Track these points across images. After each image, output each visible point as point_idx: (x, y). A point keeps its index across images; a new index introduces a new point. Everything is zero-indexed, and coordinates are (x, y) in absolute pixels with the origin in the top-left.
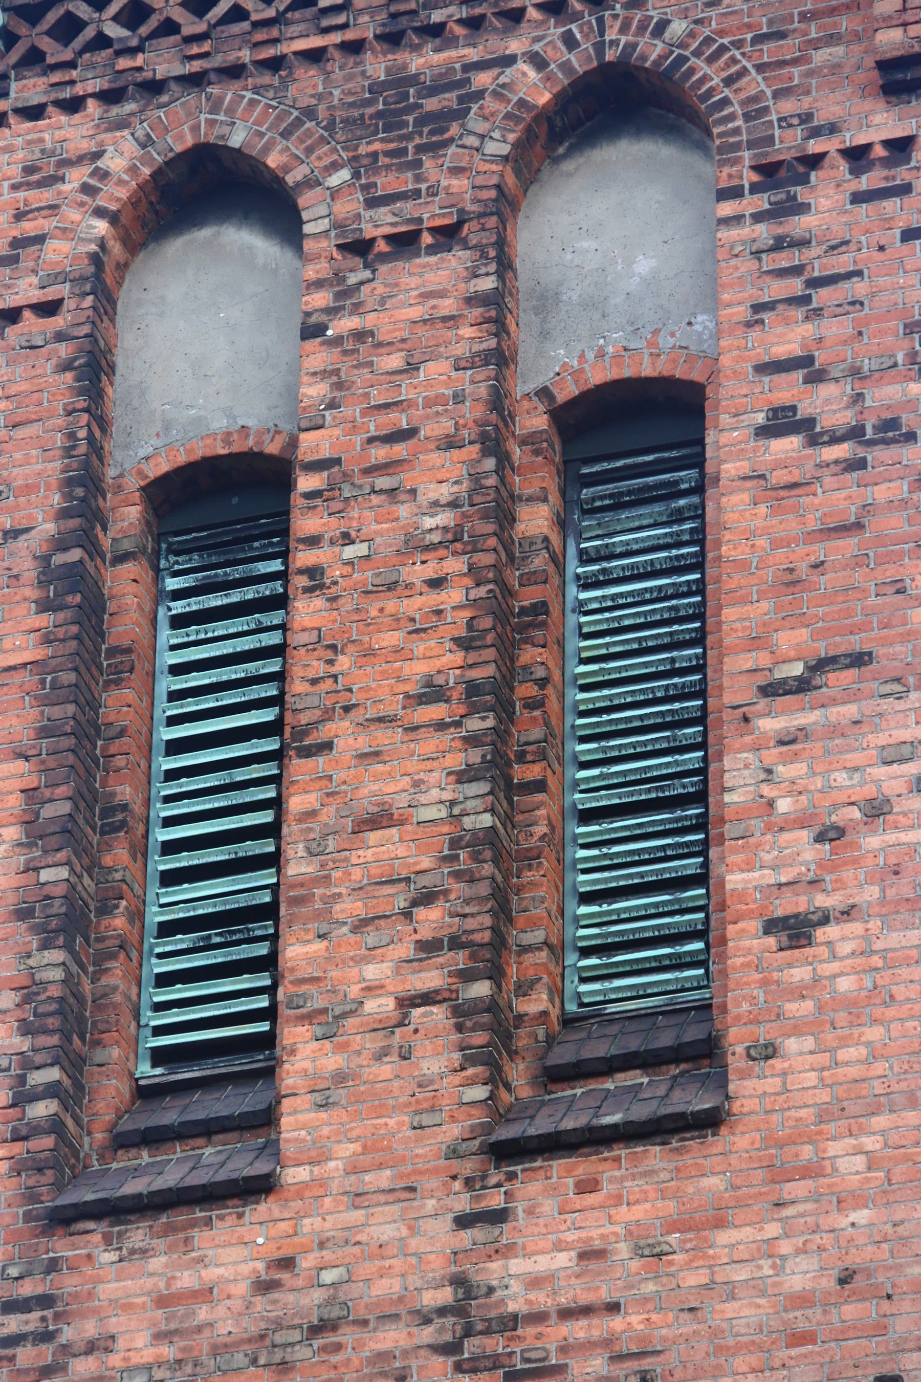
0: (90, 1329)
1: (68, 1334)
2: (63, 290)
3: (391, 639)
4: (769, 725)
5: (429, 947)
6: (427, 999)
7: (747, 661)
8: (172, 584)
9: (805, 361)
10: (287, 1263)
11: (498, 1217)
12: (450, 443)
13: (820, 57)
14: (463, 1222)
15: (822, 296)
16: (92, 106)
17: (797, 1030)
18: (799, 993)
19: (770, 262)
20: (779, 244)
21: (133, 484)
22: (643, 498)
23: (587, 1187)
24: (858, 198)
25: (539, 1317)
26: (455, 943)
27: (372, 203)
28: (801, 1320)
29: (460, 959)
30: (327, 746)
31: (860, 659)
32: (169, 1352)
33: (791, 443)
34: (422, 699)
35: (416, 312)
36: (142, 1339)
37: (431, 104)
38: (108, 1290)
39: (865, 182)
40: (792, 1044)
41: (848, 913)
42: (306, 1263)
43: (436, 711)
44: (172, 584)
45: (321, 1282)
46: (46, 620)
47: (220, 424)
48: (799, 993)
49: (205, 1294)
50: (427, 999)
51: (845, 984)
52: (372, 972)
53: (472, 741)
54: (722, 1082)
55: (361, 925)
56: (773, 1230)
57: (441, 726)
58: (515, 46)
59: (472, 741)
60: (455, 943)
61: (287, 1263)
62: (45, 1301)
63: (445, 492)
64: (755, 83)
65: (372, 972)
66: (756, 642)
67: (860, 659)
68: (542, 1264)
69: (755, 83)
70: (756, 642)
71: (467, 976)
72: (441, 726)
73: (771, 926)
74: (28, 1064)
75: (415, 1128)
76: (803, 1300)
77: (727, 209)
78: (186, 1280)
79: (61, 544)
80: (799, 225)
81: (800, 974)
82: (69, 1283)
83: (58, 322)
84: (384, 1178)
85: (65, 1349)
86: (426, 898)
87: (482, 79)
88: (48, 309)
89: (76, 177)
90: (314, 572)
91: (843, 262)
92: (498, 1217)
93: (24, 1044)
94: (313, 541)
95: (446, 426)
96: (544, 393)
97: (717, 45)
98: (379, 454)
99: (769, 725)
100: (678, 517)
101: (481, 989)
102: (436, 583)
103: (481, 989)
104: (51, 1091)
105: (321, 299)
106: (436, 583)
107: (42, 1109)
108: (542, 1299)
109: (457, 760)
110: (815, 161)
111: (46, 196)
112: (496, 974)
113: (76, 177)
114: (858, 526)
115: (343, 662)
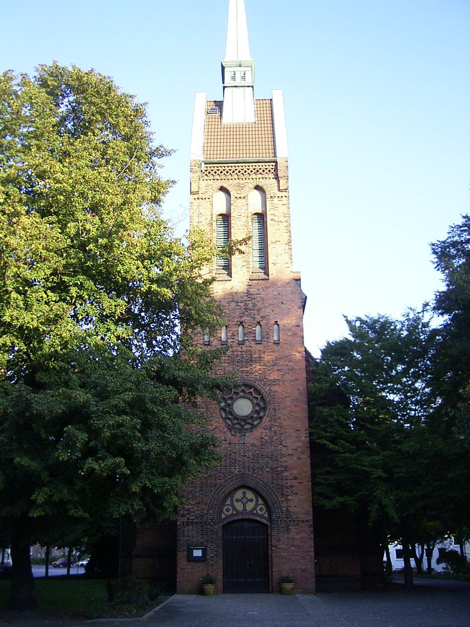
19: (271, 205)
28: (275, 297)
45: (273, 91)
68: (254, 290)
76: (276, 295)
80: (273, 202)
83: (210, 200)
87: (246, 184)
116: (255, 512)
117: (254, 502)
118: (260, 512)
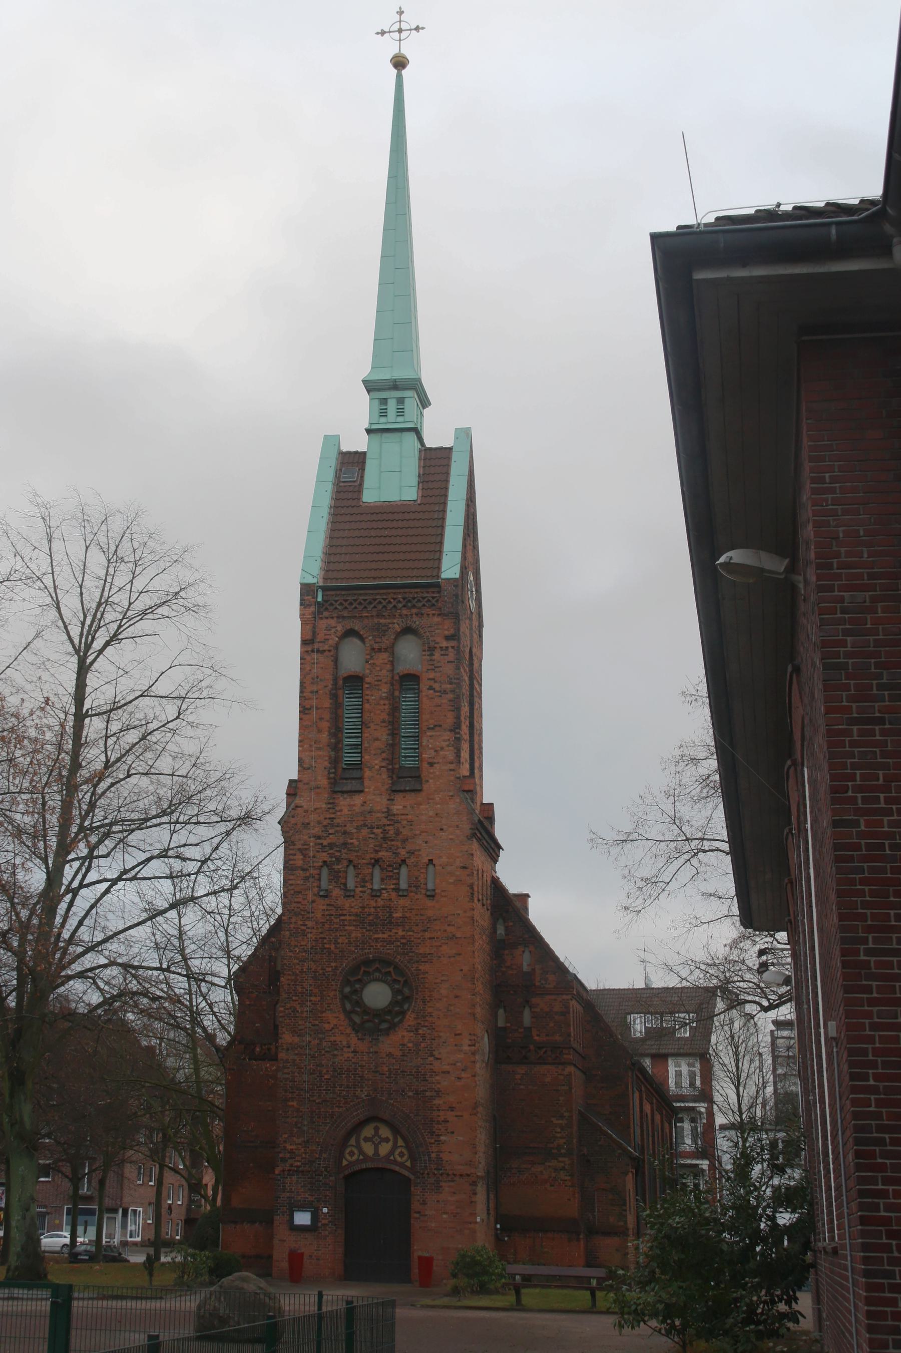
0: (339, 808)
1: (337, 808)
2: (332, 648)
3: (378, 712)
4: (428, 734)
5: (384, 759)
6: (383, 767)
7: (427, 724)
8: (347, 692)
9: (434, 679)
10: (365, 802)
11: (393, 800)
12: (386, 683)
13: (437, 631)
14: (388, 800)
15: (436, 669)
16: (335, 619)
17: (431, 779)
18: (431, 773)
20: (431, 660)
21: (341, 678)
22: (410, 689)
23: (404, 797)
24: (442, 655)
25: (398, 815)
26: (387, 759)
27: (375, 643)
29: (388, 762)
30: (369, 727)
31: (440, 726)
32: (350, 813)
33: (432, 691)
34: (382, 722)
35: (381, 661)
36: (346, 810)
37: (383, 628)
38: (342, 803)
39: (442, 652)
40: (431, 781)
41: (438, 763)
42: (368, 803)
43: (384, 724)
44: (347, 692)
46: (331, 701)
47: (353, 670)
48: (431, 773)
49: (354, 805)
50: (383, 767)
51: (437, 773)
52: (376, 762)
53: (389, 729)
54: (421, 784)
55: (375, 754)
56: (427, 807)
57: (385, 727)
58: (395, 621)
59: (389, 729)
60: (387, 759)
61: (365, 802)
62: (333, 803)
63: (386, 691)
64: (428, 634)
65: (376, 762)
66: (427, 721)
67: (440, 726)
69: (428, 634)
70: (427, 721)
71: (388, 764)
72: (385, 727)
73: (428, 763)
74: (330, 768)
75: (440, 1059)
76: (431, 817)
77: (424, 653)
78: (352, 803)
79: (332, 689)
80: (434, 657)
81: (431, 771)
82: (336, 801)
84: (378, 792)
85: (336, 811)
86: (383, 752)
87: (390, 625)
88: (329, 651)
89: (333, 630)
90: (368, 700)
91: (439, 665)
92: (393, 800)
93: (329, 765)
94: (367, 695)
95: (386, 680)
96: (398, 674)
97: (873, 1336)
98: (376, 683)
99: (428, 734)
100: (415, 693)
101: (390, 767)
102: (384, 705)
103: (390, 767)
104: (333, 773)
105: (368, 657)
106: (384, 705)
107: (332, 775)
108: (398, 812)
109: (388, 732)
110: (436, 647)
111: (329, 633)
112: (392, 765)
113: (333, 630)
114: (440, 706)
115: (372, 714)
116: (392, 1158)
117: (391, 1143)
118: (399, 1159)
